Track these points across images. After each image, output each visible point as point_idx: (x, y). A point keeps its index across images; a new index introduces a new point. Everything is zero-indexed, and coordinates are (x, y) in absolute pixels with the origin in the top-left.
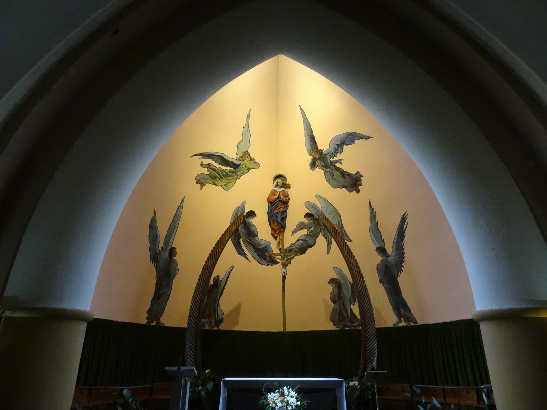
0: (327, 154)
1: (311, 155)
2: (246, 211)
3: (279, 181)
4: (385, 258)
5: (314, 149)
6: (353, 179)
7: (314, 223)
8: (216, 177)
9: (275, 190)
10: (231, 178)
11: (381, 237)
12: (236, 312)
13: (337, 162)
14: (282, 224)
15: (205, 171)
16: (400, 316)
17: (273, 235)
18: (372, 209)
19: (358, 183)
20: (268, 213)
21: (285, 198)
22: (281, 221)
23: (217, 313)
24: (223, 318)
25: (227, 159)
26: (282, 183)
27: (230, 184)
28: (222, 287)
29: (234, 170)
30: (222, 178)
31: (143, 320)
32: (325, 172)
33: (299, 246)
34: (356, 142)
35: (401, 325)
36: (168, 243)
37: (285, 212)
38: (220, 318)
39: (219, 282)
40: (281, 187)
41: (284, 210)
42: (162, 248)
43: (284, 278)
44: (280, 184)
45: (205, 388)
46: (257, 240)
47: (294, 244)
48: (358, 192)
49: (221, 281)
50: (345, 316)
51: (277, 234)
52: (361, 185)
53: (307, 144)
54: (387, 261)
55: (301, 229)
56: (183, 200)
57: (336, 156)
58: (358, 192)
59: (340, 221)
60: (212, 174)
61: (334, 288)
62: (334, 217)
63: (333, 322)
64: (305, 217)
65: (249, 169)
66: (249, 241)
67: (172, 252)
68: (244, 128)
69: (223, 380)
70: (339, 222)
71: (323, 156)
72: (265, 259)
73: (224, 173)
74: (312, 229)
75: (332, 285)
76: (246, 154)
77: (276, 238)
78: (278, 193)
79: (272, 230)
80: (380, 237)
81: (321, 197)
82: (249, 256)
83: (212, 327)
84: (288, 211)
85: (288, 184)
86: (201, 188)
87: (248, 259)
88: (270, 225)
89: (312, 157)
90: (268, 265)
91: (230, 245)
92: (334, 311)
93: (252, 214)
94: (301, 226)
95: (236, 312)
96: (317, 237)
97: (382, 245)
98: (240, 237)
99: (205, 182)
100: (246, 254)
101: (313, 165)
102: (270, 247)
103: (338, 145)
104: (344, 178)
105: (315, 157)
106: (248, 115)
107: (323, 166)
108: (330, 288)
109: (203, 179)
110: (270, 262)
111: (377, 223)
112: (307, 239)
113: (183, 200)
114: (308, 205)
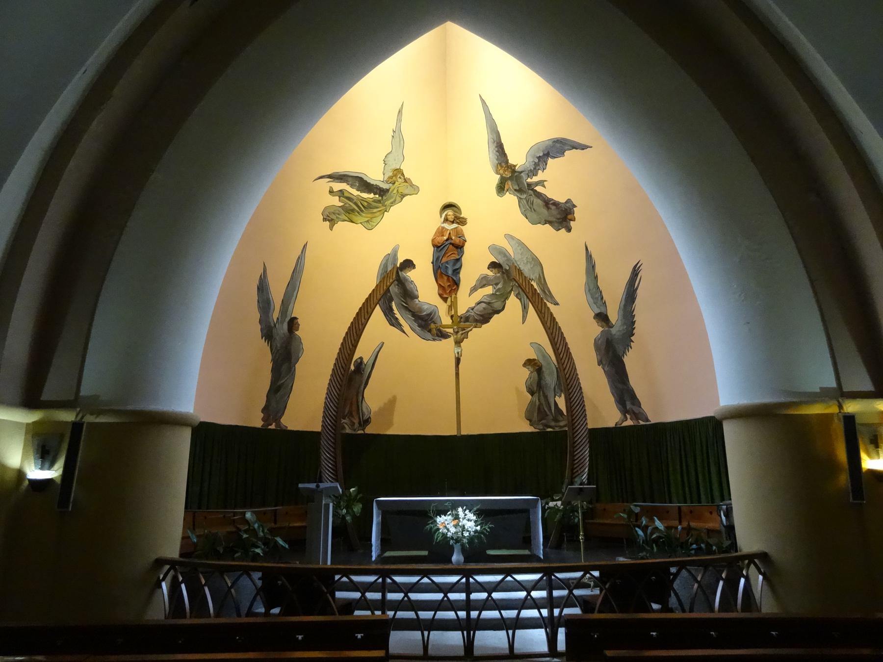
0: (521, 172)
1: (497, 173)
2: (400, 260)
3: (450, 212)
4: (607, 329)
5: (503, 164)
7: (503, 278)
8: (353, 210)
9: (443, 228)
10: (375, 210)
11: (602, 298)
12: (391, 405)
15: (336, 201)
16: (625, 411)
17: (441, 295)
18: (589, 257)
19: (569, 217)
20: (432, 263)
22: (453, 274)
23: (362, 410)
24: (370, 417)
25: (368, 181)
26: (453, 217)
27: (374, 220)
29: (380, 198)
31: (258, 423)
32: (520, 199)
33: (480, 312)
34: (567, 153)
35: (625, 424)
37: (458, 260)
38: (366, 417)
40: (453, 222)
41: (458, 257)
42: (278, 319)
43: (458, 361)
44: (451, 218)
45: (350, 511)
46: (417, 304)
47: (473, 309)
48: (569, 230)
49: (365, 365)
50: (548, 413)
51: (446, 294)
52: (574, 220)
53: (491, 155)
55: (483, 286)
56: (305, 246)
57: (536, 175)
58: (569, 230)
59: (541, 275)
60: (347, 205)
61: (532, 372)
63: (530, 421)
64: (488, 268)
65: (403, 196)
67: (293, 324)
68: (394, 132)
69: (379, 502)
71: (516, 174)
72: (430, 331)
73: (365, 204)
74: (500, 286)
75: (528, 369)
76: (398, 172)
77: (445, 300)
82: (406, 327)
83: (355, 430)
84: (463, 258)
86: (331, 228)
87: (404, 332)
89: (499, 176)
90: (434, 340)
91: (378, 313)
92: (532, 403)
93: (408, 264)
94: (483, 282)
96: (507, 298)
97: (603, 310)
98: (391, 300)
99: (337, 217)
100: (401, 325)
101: (501, 189)
103: (539, 158)
104: (548, 208)
105: (504, 175)
106: (400, 112)
107: (515, 190)
108: (526, 373)
109: (334, 213)
111: (596, 278)
112: (493, 301)
113: (305, 246)
114: (493, 249)
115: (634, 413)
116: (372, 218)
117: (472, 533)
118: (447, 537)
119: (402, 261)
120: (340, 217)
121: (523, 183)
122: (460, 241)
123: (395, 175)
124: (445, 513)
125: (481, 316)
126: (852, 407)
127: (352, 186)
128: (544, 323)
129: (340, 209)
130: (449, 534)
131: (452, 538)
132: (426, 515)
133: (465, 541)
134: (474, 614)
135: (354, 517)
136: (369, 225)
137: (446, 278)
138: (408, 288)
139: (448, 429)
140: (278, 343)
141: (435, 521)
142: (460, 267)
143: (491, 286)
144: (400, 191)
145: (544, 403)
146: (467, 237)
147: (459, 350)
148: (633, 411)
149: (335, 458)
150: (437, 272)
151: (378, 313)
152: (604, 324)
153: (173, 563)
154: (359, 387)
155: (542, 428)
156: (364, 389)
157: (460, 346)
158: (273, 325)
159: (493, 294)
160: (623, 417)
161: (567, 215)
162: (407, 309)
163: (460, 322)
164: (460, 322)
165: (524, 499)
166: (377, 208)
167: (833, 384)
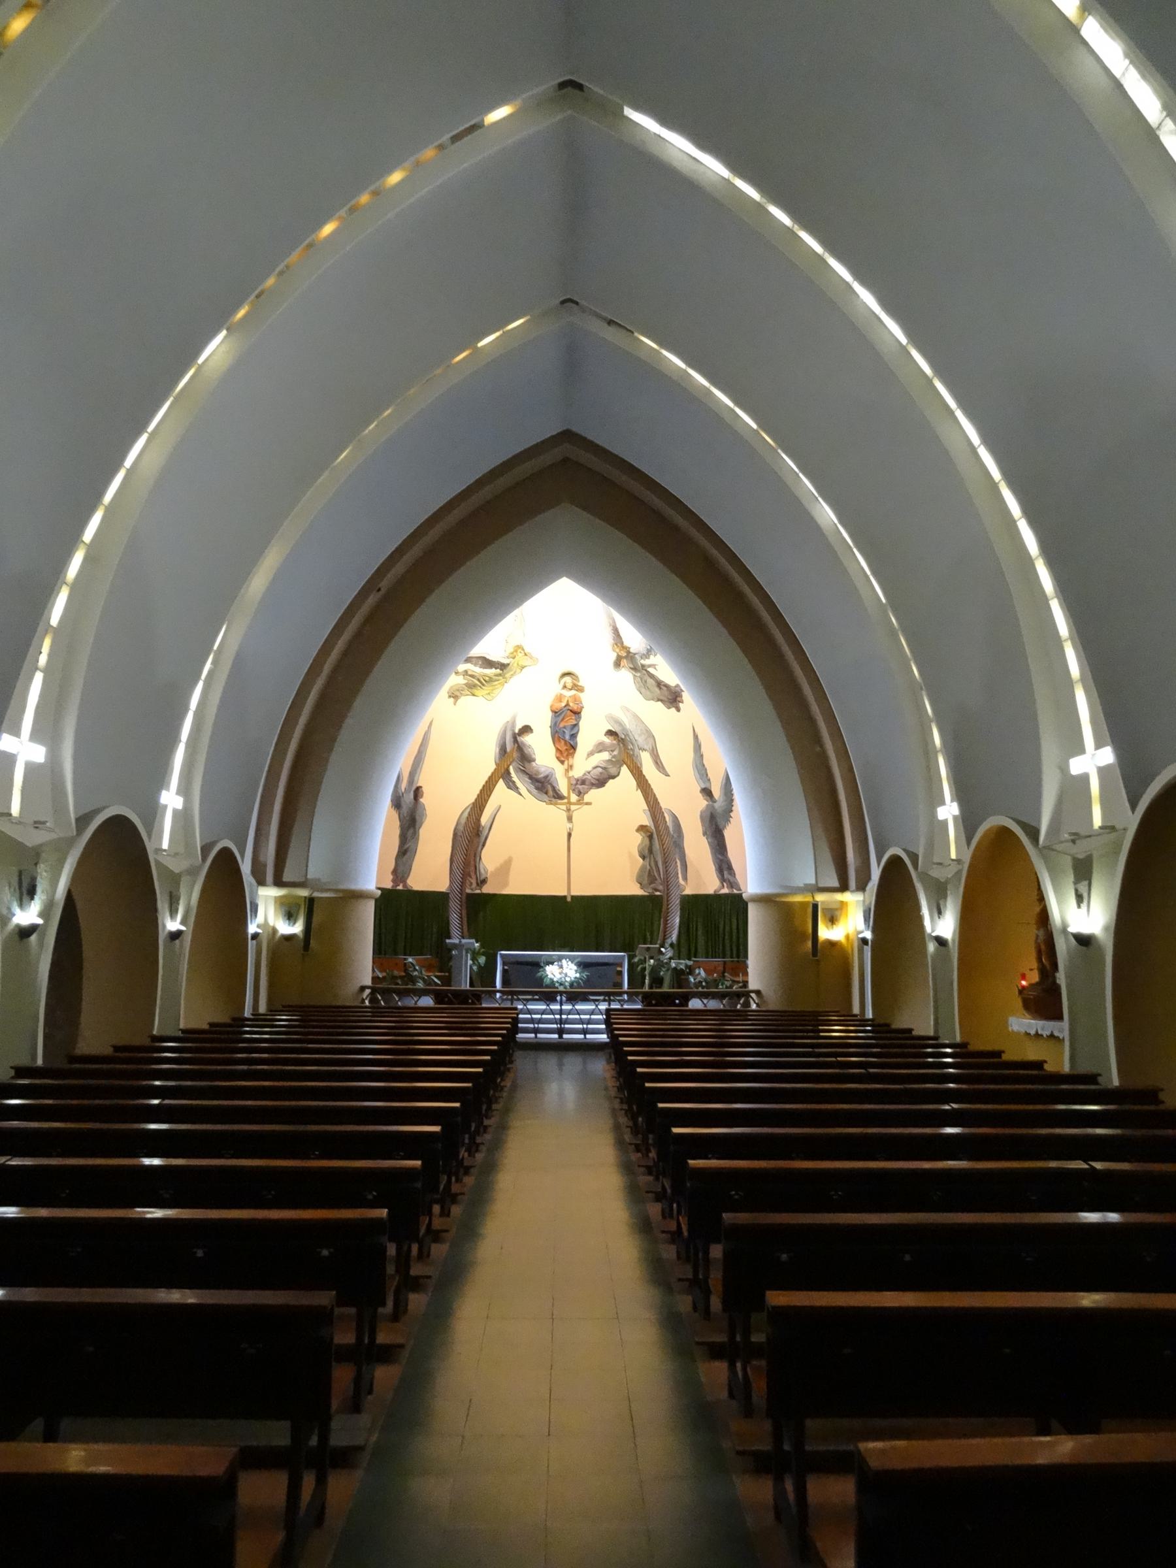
0: (635, 654)
1: (614, 651)
3: (568, 679)
5: (619, 644)
6: (672, 692)
9: (561, 694)
10: (496, 683)
11: (707, 775)
12: (505, 868)
13: (650, 666)
14: (572, 743)
16: (723, 880)
18: (696, 737)
19: (679, 699)
20: (551, 727)
21: (576, 705)
22: (570, 739)
23: (479, 870)
26: (571, 684)
27: (494, 692)
28: (485, 837)
30: (483, 685)
33: (597, 775)
36: (413, 782)
37: (576, 725)
38: (482, 878)
39: (481, 829)
40: (571, 689)
41: (575, 722)
43: (569, 835)
44: (569, 685)
45: (476, 962)
47: (589, 773)
48: (678, 710)
49: (483, 828)
50: (657, 877)
51: (563, 757)
52: (682, 702)
54: (713, 807)
55: (600, 751)
56: (431, 724)
57: (649, 658)
58: (678, 710)
59: (654, 747)
60: (470, 682)
62: (646, 739)
63: (641, 884)
65: (523, 667)
66: (522, 768)
67: (418, 792)
69: (501, 954)
70: (653, 748)
72: (546, 793)
73: (487, 679)
74: (615, 753)
75: (641, 835)
77: (562, 762)
78: (566, 699)
79: (556, 751)
80: (705, 775)
81: (628, 710)
83: (472, 889)
85: (581, 686)
87: (521, 795)
88: (554, 743)
89: (615, 654)
91: (501, 784)
92: (642, 869)
93: (526, 729)
94: (600, 748)
95: (505, 868)
99: (461, 694)
100: (517, 788)
101: (617, 664)
102: (553, 776)
104: (660, 688)
105: (620, 654)
107: (630, 668)
109: (458, 690)
110: (554, 797)
111: (702, 756)
113: (431, 724)
115: (731, 883)
116: (493, 690)
117: (573, 979)
118: (553, 981)
119: (520, 727)
120: (463, 692)
121: (638, 664)
122: (578, 708)
123: (516, 651)
124: (552, 963)
125: (598, 780)
126: (820, 898)
127: (475, 665)
128: (648, 802)
129: (464, 686)
130: (555, 980)
131: (557, 982)
132: (537, 965)
133: (567, 984)
134: (564, 1017)
135: (479, 967)
136: (489, 697)
137: (563, 742)
138: (526, 752)
139: (556, 889)
140: (405, 810)
141: (545, 970)
142: (577, 733)
143: (607, 752)
144: (520, 664)
145: (654, 868)
146: (585, 704)
147: (571, 826)
148: (729, 881)
149: (461, 918)
150: (555, 737)
151: (501, 784)
152: (708, 798)
153: (368, 987)
154: (478, 847)
155: (651, 891)
156: (482, 849)
157: (572, 822)
158: (401, 795)
159: (609, 760)
160: (721, 885)
161: (677, 697)
162: (524, 772)
163: (577, 784)
164: (577, 784)
165: (618, 955)
166: (498, 680)
167: (813, 881)
